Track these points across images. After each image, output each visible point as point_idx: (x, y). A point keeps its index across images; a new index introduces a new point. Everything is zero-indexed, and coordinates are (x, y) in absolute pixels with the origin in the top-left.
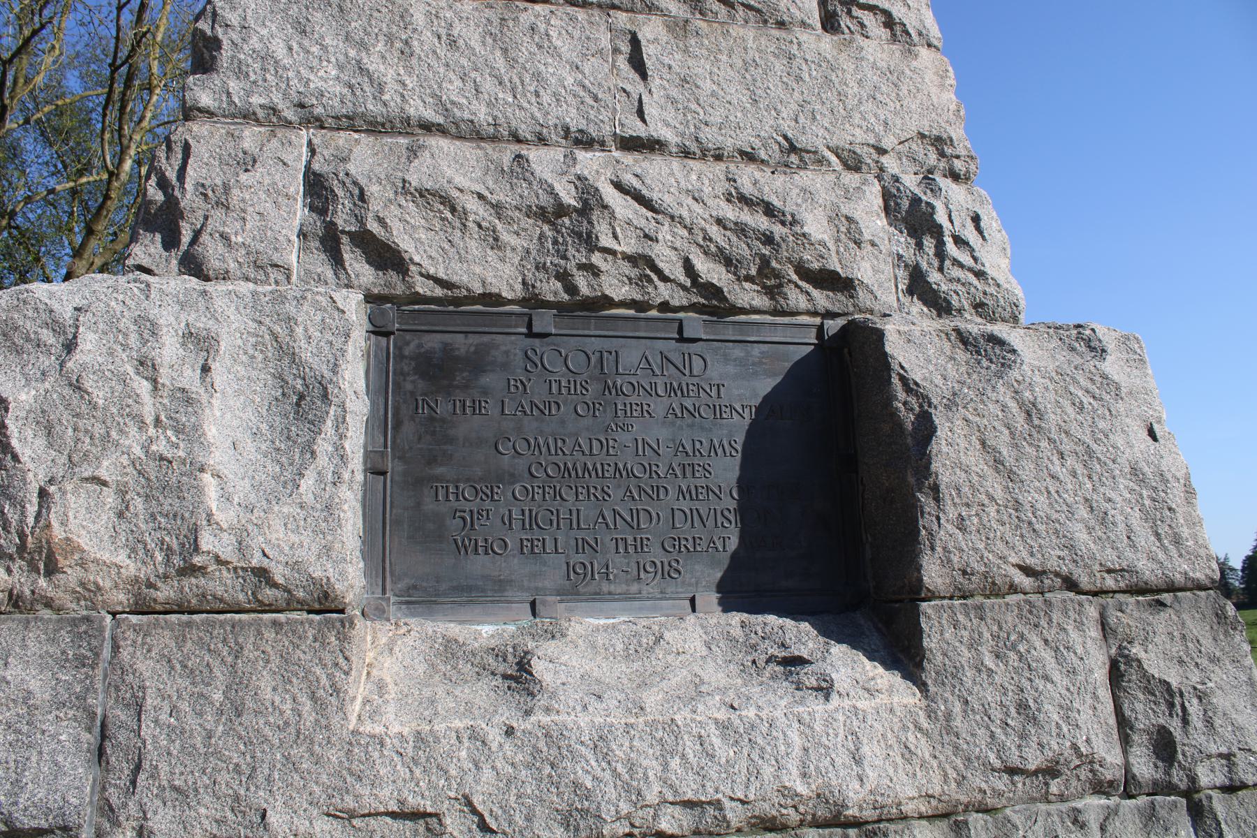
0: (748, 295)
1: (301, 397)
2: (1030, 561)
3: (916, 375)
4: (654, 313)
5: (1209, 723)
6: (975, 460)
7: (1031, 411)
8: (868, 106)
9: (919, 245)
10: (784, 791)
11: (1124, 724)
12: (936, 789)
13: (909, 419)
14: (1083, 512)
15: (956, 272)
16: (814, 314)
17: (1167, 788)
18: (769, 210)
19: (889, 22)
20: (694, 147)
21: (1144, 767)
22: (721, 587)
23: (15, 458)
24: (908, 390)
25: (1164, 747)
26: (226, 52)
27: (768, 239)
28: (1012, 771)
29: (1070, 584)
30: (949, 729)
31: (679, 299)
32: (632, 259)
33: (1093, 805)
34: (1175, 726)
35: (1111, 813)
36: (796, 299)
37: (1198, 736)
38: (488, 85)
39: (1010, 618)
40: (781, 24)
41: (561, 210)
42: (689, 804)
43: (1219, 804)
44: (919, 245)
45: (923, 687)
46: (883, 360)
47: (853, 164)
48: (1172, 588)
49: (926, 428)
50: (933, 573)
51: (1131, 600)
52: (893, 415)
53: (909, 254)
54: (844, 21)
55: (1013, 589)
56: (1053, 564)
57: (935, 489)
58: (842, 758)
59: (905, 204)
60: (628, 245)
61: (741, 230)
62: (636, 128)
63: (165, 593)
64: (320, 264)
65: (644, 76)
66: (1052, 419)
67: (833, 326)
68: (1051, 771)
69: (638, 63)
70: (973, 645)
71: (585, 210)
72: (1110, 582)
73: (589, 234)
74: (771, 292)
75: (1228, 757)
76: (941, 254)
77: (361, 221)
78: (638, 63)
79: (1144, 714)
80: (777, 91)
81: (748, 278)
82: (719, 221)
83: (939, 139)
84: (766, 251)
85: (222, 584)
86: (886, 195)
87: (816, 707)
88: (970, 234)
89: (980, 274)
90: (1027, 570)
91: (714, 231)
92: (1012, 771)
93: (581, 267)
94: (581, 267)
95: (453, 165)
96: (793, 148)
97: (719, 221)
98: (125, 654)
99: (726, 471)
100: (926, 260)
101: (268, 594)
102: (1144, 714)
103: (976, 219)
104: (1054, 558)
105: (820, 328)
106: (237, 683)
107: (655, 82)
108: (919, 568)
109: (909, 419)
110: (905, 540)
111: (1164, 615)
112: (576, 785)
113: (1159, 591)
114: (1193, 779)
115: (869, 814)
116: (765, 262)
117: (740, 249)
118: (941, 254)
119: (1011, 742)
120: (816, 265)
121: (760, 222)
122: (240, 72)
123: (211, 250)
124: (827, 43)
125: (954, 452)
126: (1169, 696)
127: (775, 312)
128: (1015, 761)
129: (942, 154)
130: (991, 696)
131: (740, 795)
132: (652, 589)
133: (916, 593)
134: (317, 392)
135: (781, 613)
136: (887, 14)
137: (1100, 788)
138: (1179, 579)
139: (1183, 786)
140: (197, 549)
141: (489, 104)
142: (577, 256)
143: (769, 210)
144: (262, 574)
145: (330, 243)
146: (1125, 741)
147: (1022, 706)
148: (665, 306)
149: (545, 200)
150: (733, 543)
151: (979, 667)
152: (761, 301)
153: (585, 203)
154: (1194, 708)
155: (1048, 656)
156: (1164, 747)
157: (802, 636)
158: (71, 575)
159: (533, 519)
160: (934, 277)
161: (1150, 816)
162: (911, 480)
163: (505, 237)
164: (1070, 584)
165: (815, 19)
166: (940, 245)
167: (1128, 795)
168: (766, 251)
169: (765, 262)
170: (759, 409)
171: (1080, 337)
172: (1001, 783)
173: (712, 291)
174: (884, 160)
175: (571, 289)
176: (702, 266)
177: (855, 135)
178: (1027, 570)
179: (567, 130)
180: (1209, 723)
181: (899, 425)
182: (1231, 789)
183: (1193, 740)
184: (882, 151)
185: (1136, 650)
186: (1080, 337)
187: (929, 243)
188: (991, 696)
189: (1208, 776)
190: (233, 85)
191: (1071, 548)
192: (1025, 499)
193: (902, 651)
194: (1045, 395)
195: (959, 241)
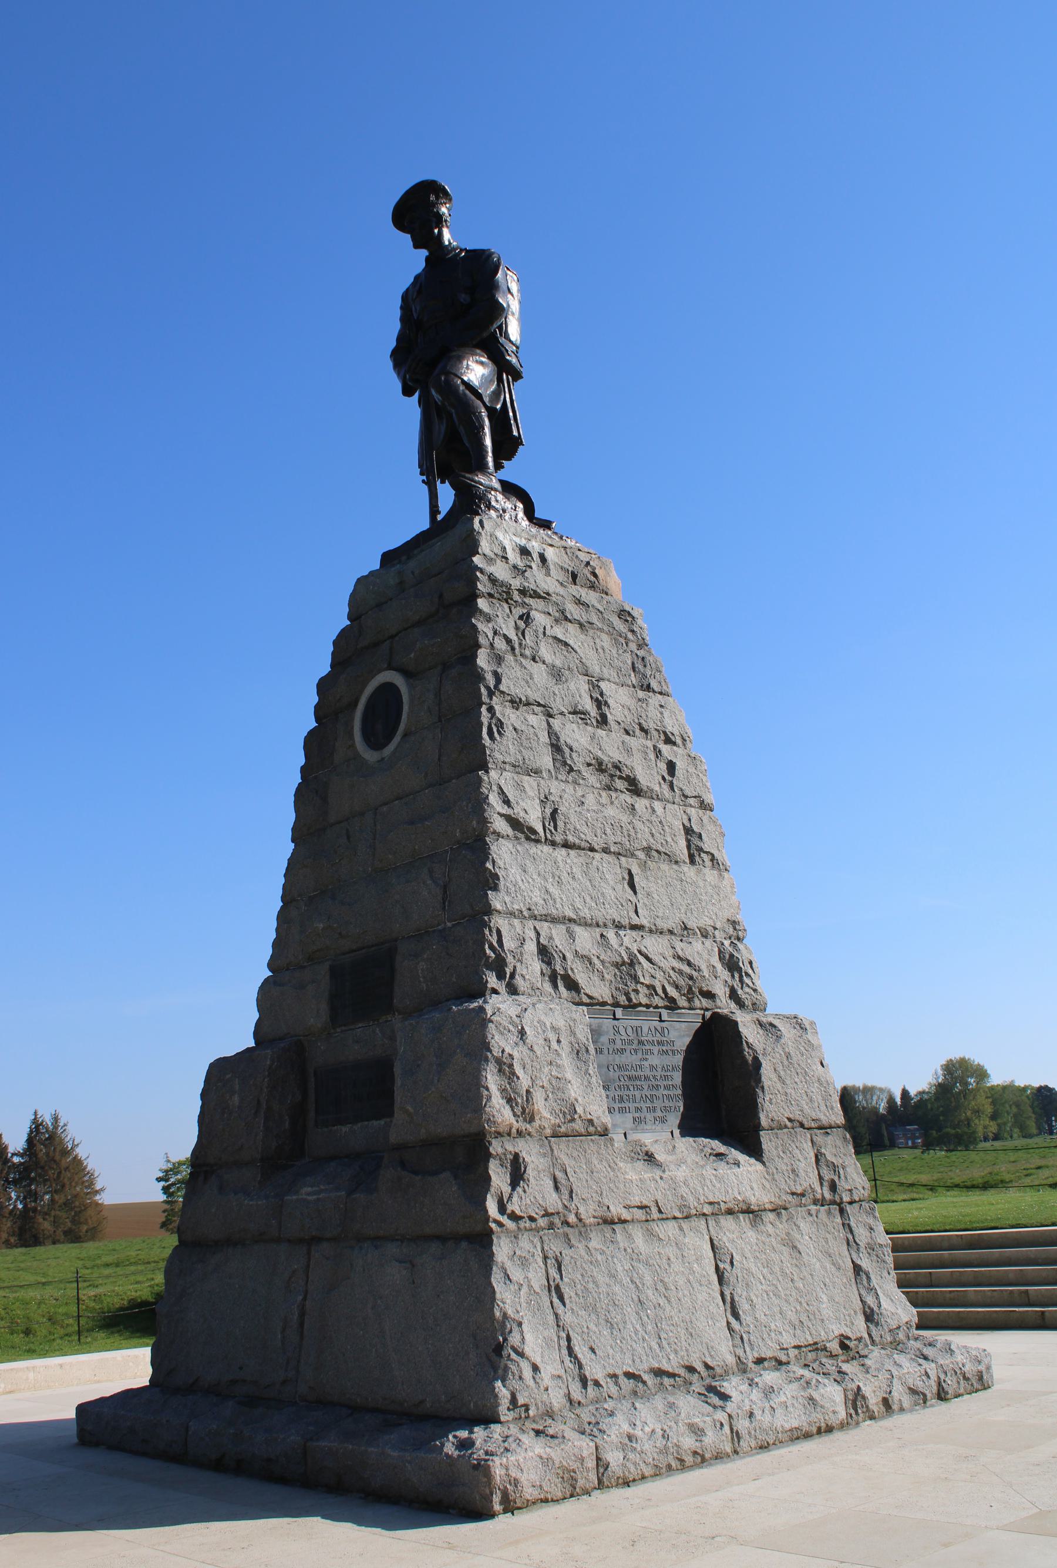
0: (682, 1002)
1: (578, 1052)
2: (791, 1116)
3: (750, 1041)
4: (651, 1009)
5: (846, 1178)
6: (774, 1077)
7: (788, 1056)
8: (710, 907)
9: (733, 976)
10: (735, 1199)
11: (821, 1178)
12: (773, 1200)
13: (750, 1059)
14: (805, 1097)
15: (747, 990)
16: (701, 1009)
17: (833, 1202)
18: (689, 964)
19: (713, 858)
20: (653, 928)
21: (828, 1195)
22: (680, 1127)
23: (518, 1078)
24: (749, 1047)
25: (833, 1187)
26: (502, 882)
27: (691, 978)
28: (793, 1194)
29: (802, 1125)
30: (774, 1179)
31: (661, 1003)
32: (648, 987)
33: (813, 1208)
34: (836, 1179)
35: (818, 1211)
36: (697, 1003)
37: (843, 1183)
38: (588, 899)
39: (785, 1137)
40: (676, 862)
41: (624, 963)
42: (711, 1203)
43: (848, 1208)
44: (733, 976)
45: (763, 1163)
46: (738, 1035)
47: (705, 936)
48: (831, 1127)
49: (757, 1064)
50: (764, 1121)
51: (819, 1131)
52: (744, 1057)
53: (729, 980)
54: (697, 858)
55: (786, 1127)
56: (797, 1117)
57: (763, 1088)
58: (748, 1188)
59: (727, 956)
60: (647, 981)
61: (681, 972)
62: (636, 921)
63: (563, 1129)
64: (548, 987)
65: (635, 893)
66: (795, 1059)
67: (708, 1014)
68: (803, 1195)
69: (632, 885)
70: (776, 1148)
71: (632, 964)
72: (813, 1125)
73: (635, 975)
74: (690, 1000)
75: (850, 1190)
76: (741, 981)
77: (565, 969)
78: (632, 885)
79: (827, 1175)
80: (680, 900)
81: (684, 995)
82: (673, 969)
83: (734, 922)
84: (691, 983)
85: (579, 1126)
86: (720, 952)
87: (736, 1170)
88: (750, 972)
89: (755, 990)
90: (790, 1120)
91: (671, 972)
92: (793, 1194)
93: (634, 990)
94: (634, 990)
95: (585, 940)
96: (686, 928)
97: (673, 969)
98: (555, 1152)
99: (677, 1077)
100: (736, 984)
101: (591, 1129)
102: (827, 1175)
103: (751, 963)
104: (797, 1115)
105: (704, 1015)
106: (588, 1162)
107: (639, 896)
108: (759, 1118)
109: (750, 1059)
110: (751, 1107)
111: (830, 1137)
112: (682, 1196)
113: (826, 1128)
114: (841, 1199)
115: (756, 1208)
116: (690, 988)
117: (681, 982)
118: (741, 981)
119: (792, 1183)
120: (705, 989)
121: (686, 969)
122: (508, 893)
123: (518, 981)
124: (693, 869)
125: (767, 1072)
126: (834, 1168)
127: (690, 1009)
128: (794, 1190)
129: (735, 929)
130: (784, 1168)
131: (76, 1338)
132: (658, 1128)
133: (758, 1127)
134: (584, 1049)
135: (706, 1137)
136: (713, 855)
137: (815, 1202)
138: (833, 1124)
139: (838, 1201)
140: (576, 1112)
141: (589, 909)
142: (632, 986)
143: (689, 964)
144: (591, 1121)
145: (553, 978)
146: (821, 1184)
147: (793, 1171)
148: (657, 1007)
149: (619, 960)
150: (682, 1109)
151: (779, 1156)
152: (685, 1004)
153: (632, 960)
154: (841, 1172)
155: (798, 1152)
156: (833, 1187)
157: (717, 1145)
158: (537, 1123)
159: (622, 1098)
160: (740, 992)
161: (829, 1212)
162: (753, 1084)
163: (606, 975)
164: (802, 1125)
165: (687, 861)
166: (741, 977)
167: (822, 1205)
168: (691, 983)
169: (690, 988)
170: (686, 1051)
171: (797, 1023)
172: (790, 1198)
173: (673, 1000)
174: (717, 932)
175: (629, 1000)
176: (669, 989)
177: (706, 922)
178: (790, 1120)
179: (614, 921)
180: (846, 1178)
181: (746, 1061)
182: (851, 1203)
183: (842, 1185)
184: (715, 929)
185: (823, 1150)
186: (797, 1023)
187: (736, 975)
188: (784, 1168)
189: (846, 1198)
190: (507, 899)
191: (802, 1111)
192: (788, 1091)
193: (754, 1150)
194: (791, 1048)
195: (747, 975)
